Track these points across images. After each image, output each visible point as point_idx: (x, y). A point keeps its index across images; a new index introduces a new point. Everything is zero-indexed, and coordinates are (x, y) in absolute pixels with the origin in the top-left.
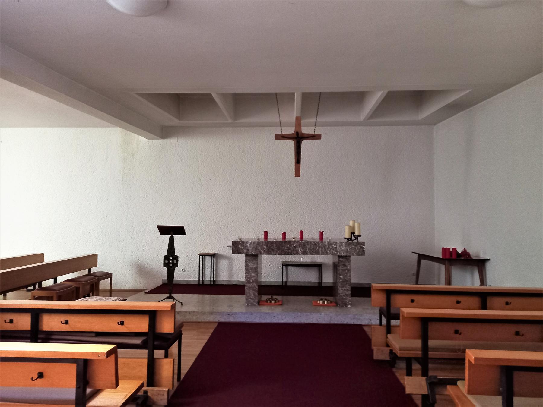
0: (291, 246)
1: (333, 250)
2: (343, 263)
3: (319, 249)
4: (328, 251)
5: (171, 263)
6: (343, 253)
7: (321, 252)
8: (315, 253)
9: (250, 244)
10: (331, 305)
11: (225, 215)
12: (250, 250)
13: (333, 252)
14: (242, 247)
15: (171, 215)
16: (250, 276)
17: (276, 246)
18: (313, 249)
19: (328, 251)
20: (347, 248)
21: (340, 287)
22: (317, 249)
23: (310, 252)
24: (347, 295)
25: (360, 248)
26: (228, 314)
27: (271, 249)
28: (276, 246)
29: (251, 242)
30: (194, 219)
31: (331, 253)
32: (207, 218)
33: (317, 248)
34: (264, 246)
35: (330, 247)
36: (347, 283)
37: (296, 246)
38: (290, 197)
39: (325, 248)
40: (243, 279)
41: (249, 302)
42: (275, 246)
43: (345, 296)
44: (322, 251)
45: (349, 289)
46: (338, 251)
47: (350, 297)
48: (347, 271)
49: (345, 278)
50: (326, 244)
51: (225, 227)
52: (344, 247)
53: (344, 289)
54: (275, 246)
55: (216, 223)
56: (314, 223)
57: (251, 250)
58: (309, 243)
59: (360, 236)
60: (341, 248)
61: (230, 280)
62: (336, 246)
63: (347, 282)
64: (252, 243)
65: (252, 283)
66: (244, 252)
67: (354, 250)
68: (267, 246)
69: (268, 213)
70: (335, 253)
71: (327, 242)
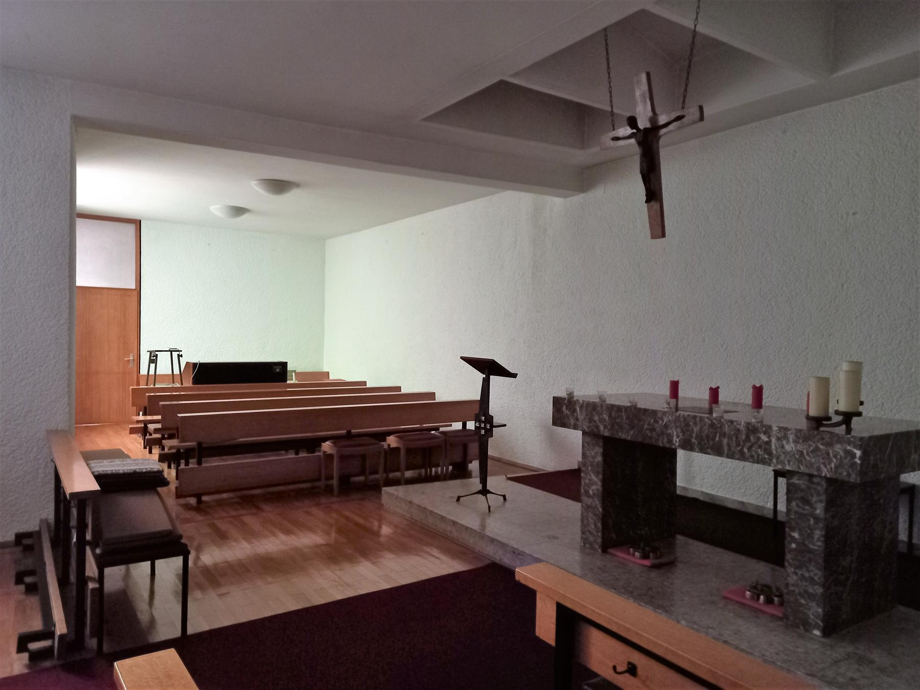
0: (657, 422)
1: (760, 447)
2: (800, 494)
3: (723, 439)
4: (746, 450)
5: (480, 425)
6: (789, 461)
7: (726, 449)
8: (712, 449)
9: (581, 407)
10: (770, 610)
11: (681, 341)
12: (580, 421)
13: (758, 455)
14: (568, 412)
15: (592, 339)
16: (590, 480)
17: (628, 418)
18: (708, 437)
19: (746, 450)
20: (800, 447)
21: (790, 564)
22: (717, 439)
23: (699, 443)
24: (811, 597)
25: (842, 454)
26: (514, 552)
27: (618, 423)
28: (626, 419)
29: (583, 403)
30: (626, 348)
31: (752, 456)
32: (648, 345)
33: (718, 435)
34: (605, 416)
35: (752, 438)
36: (810, 560)
37: (668, 423)
38: (831, 293)
39: (737, 438)
40: (714, 489)
41: (586, 539)
42: (624, 418)
43: (803, 597)
44: (729, 446)
45: (816, 578)
46: (774, 452)
47: (818, 605)
48: (812, 521)
49: (806, 543)
50: (742, 428)
51: (681, 368)
52: (792, 445)
53: (802, 575)
54: (624, 418)
55: (664, 358)
56: (902, 367)
57: (582, 420)
58: (698, 419)
59: (859, 414)
60: (783, 447)
61: (687, 486)
62: (768, 437)
63: (811, 555)
64: (585, 405)
65: (592, 497)
66: (570, 424)
67: (823, 458)
68: (610, 415)
69: (774, 338)
70: (765, 458)
71: (743, 423)
